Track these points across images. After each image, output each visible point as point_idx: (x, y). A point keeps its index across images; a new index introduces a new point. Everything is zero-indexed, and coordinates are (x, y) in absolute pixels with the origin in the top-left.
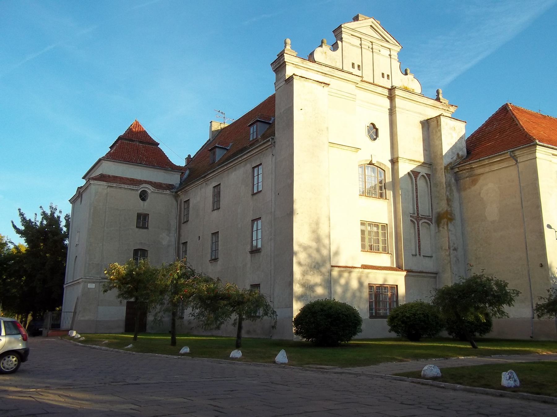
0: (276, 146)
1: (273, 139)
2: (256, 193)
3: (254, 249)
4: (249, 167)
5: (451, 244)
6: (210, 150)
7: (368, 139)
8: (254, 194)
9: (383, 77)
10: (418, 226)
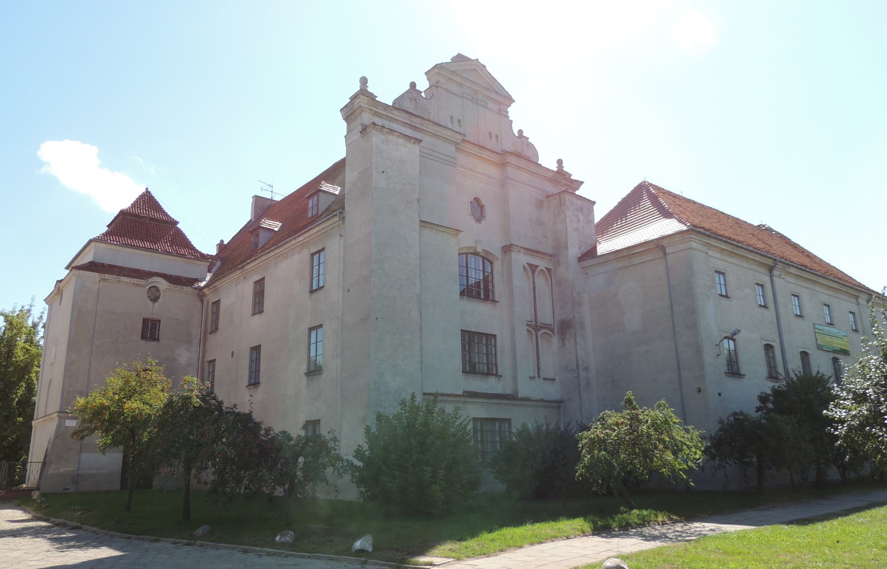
0: (346, 222)
1: (341, 213)
2: (316, 290)
3: (312, 368)
4: (306, 254)
5: (580, 362)
6: (251, 232)
7: (473, 222)
8: (312, 292)
9: (497, 136)
10: (537, 338)
